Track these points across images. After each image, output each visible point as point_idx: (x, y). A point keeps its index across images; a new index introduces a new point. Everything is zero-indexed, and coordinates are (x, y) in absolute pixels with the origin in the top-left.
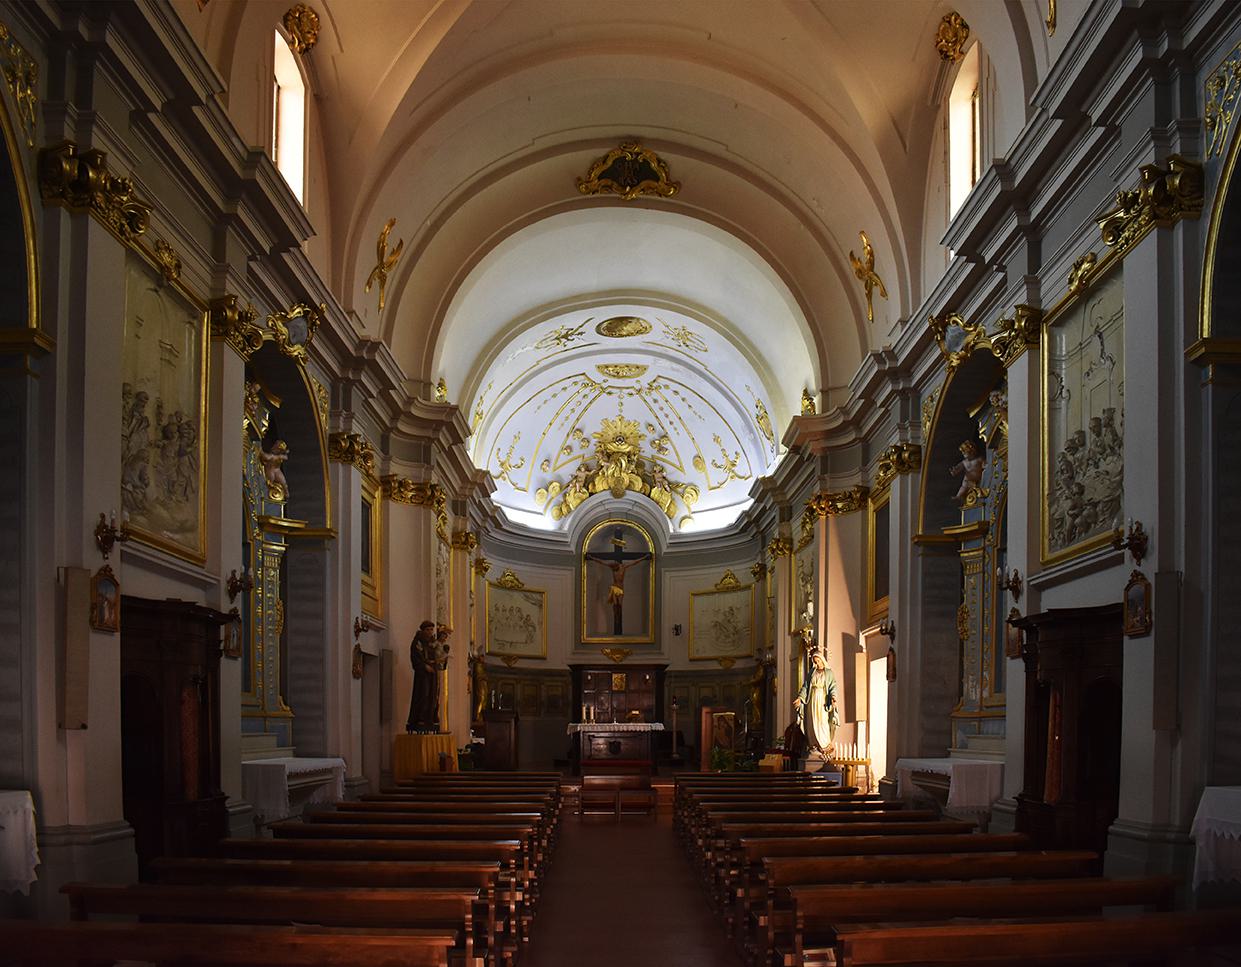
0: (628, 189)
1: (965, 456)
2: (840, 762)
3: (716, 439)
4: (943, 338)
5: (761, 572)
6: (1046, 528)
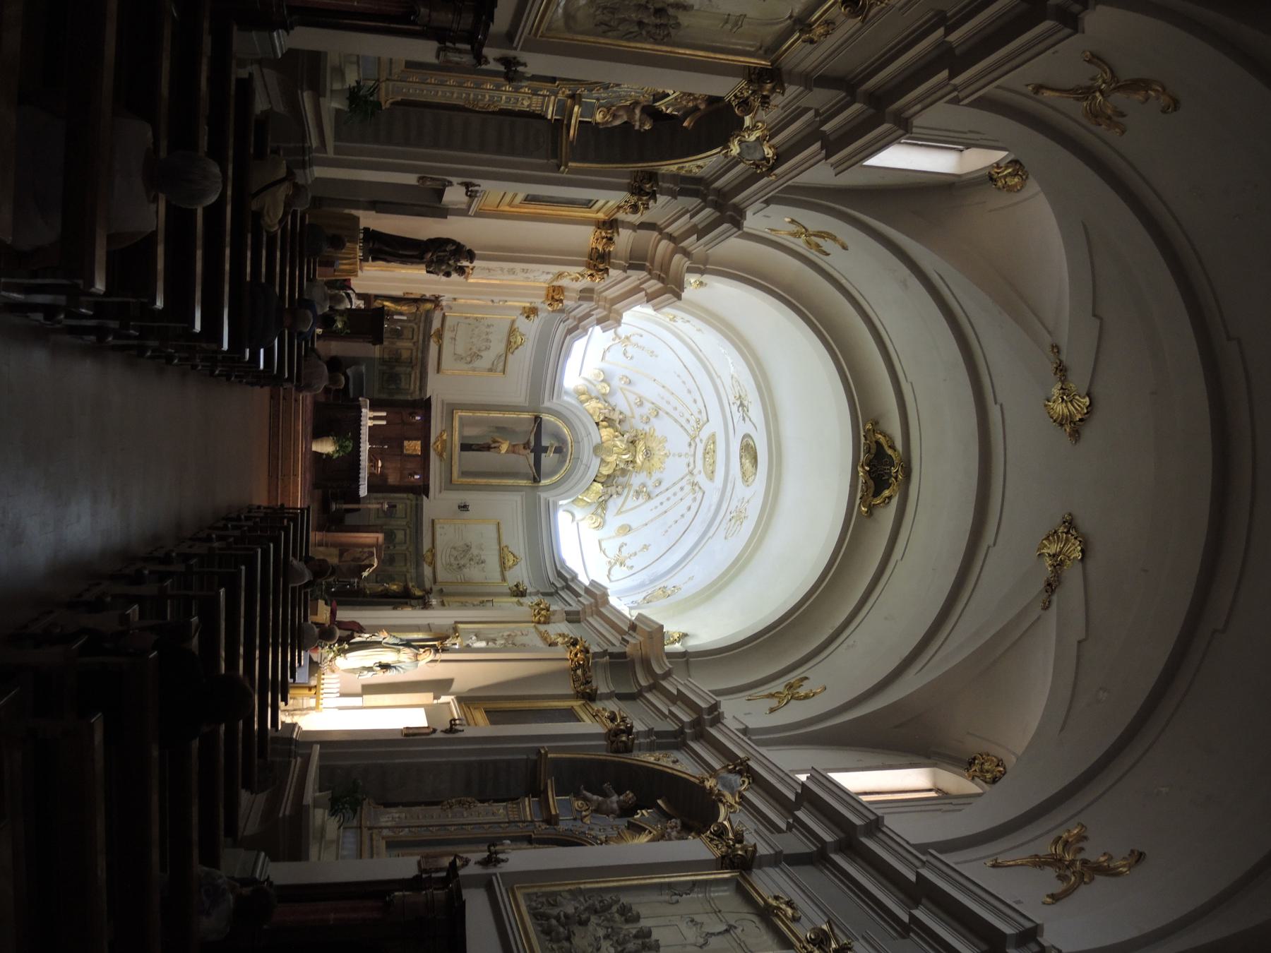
0: (867, 468)
1: (621, 798)
2: (319, 679)
3: (646, 547)
4: (730, 772)
5: (519, 592)
6: (548, 889)
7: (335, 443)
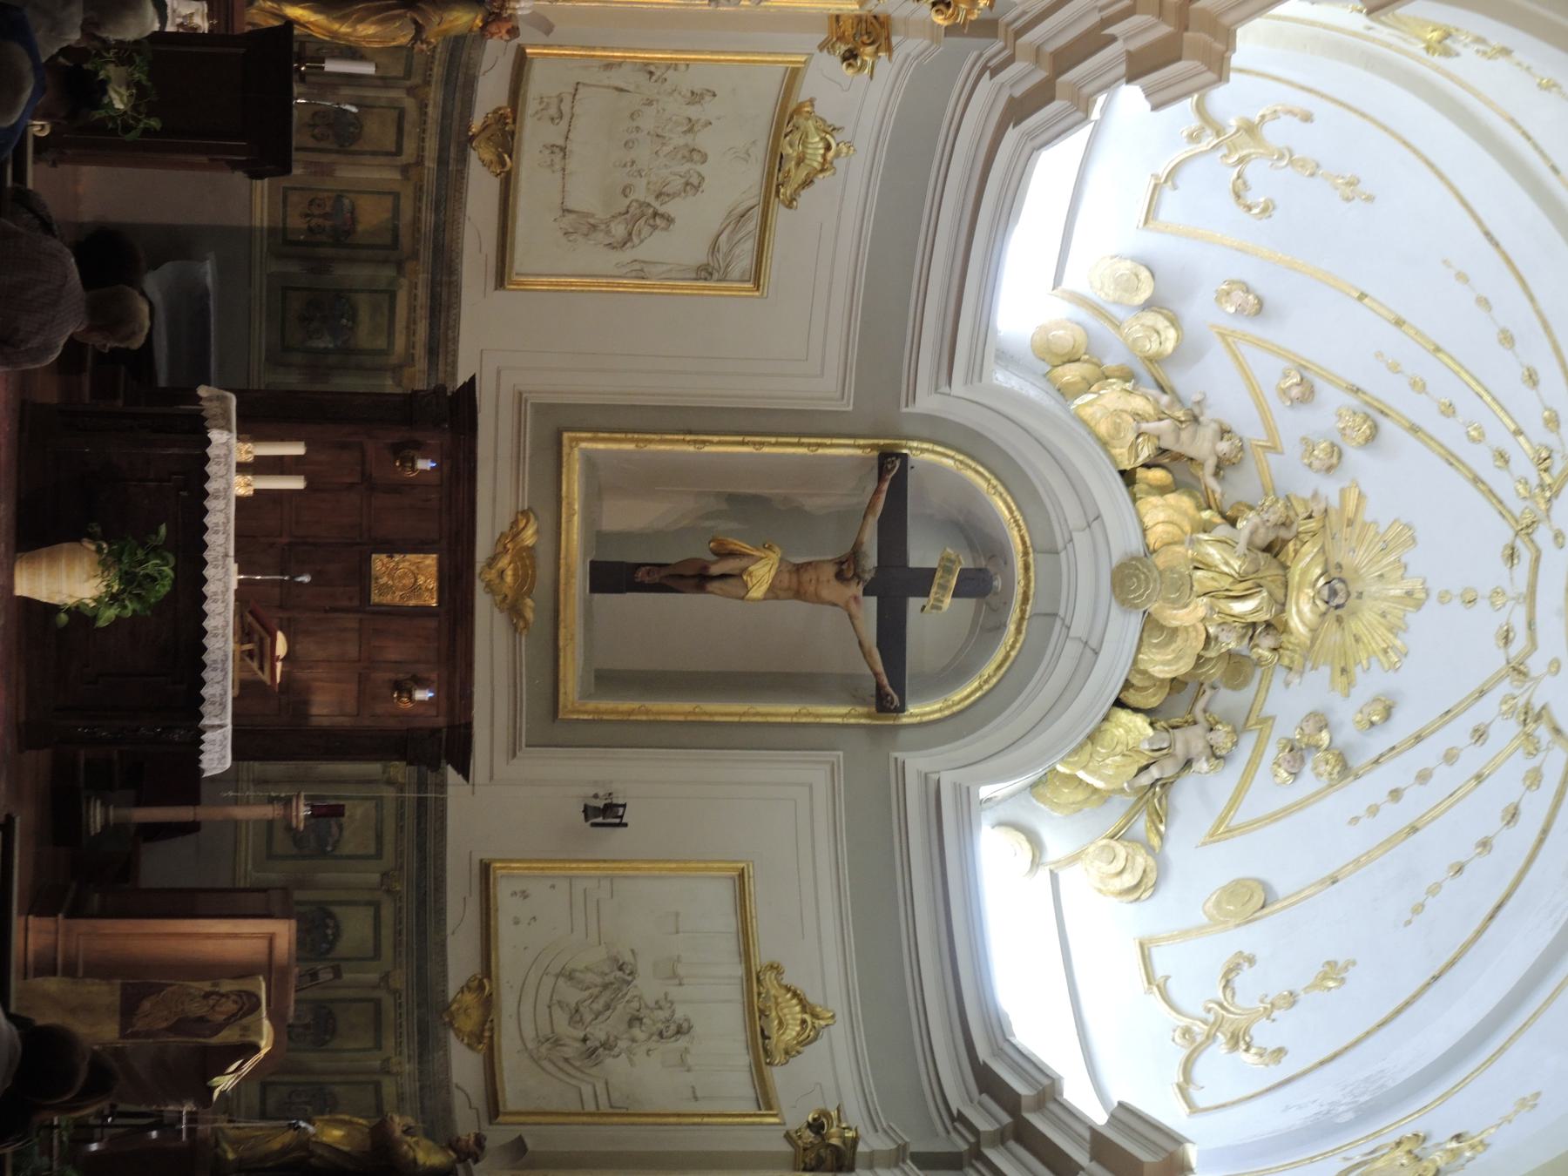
3: (1333, 972)
7: (104, 565)
